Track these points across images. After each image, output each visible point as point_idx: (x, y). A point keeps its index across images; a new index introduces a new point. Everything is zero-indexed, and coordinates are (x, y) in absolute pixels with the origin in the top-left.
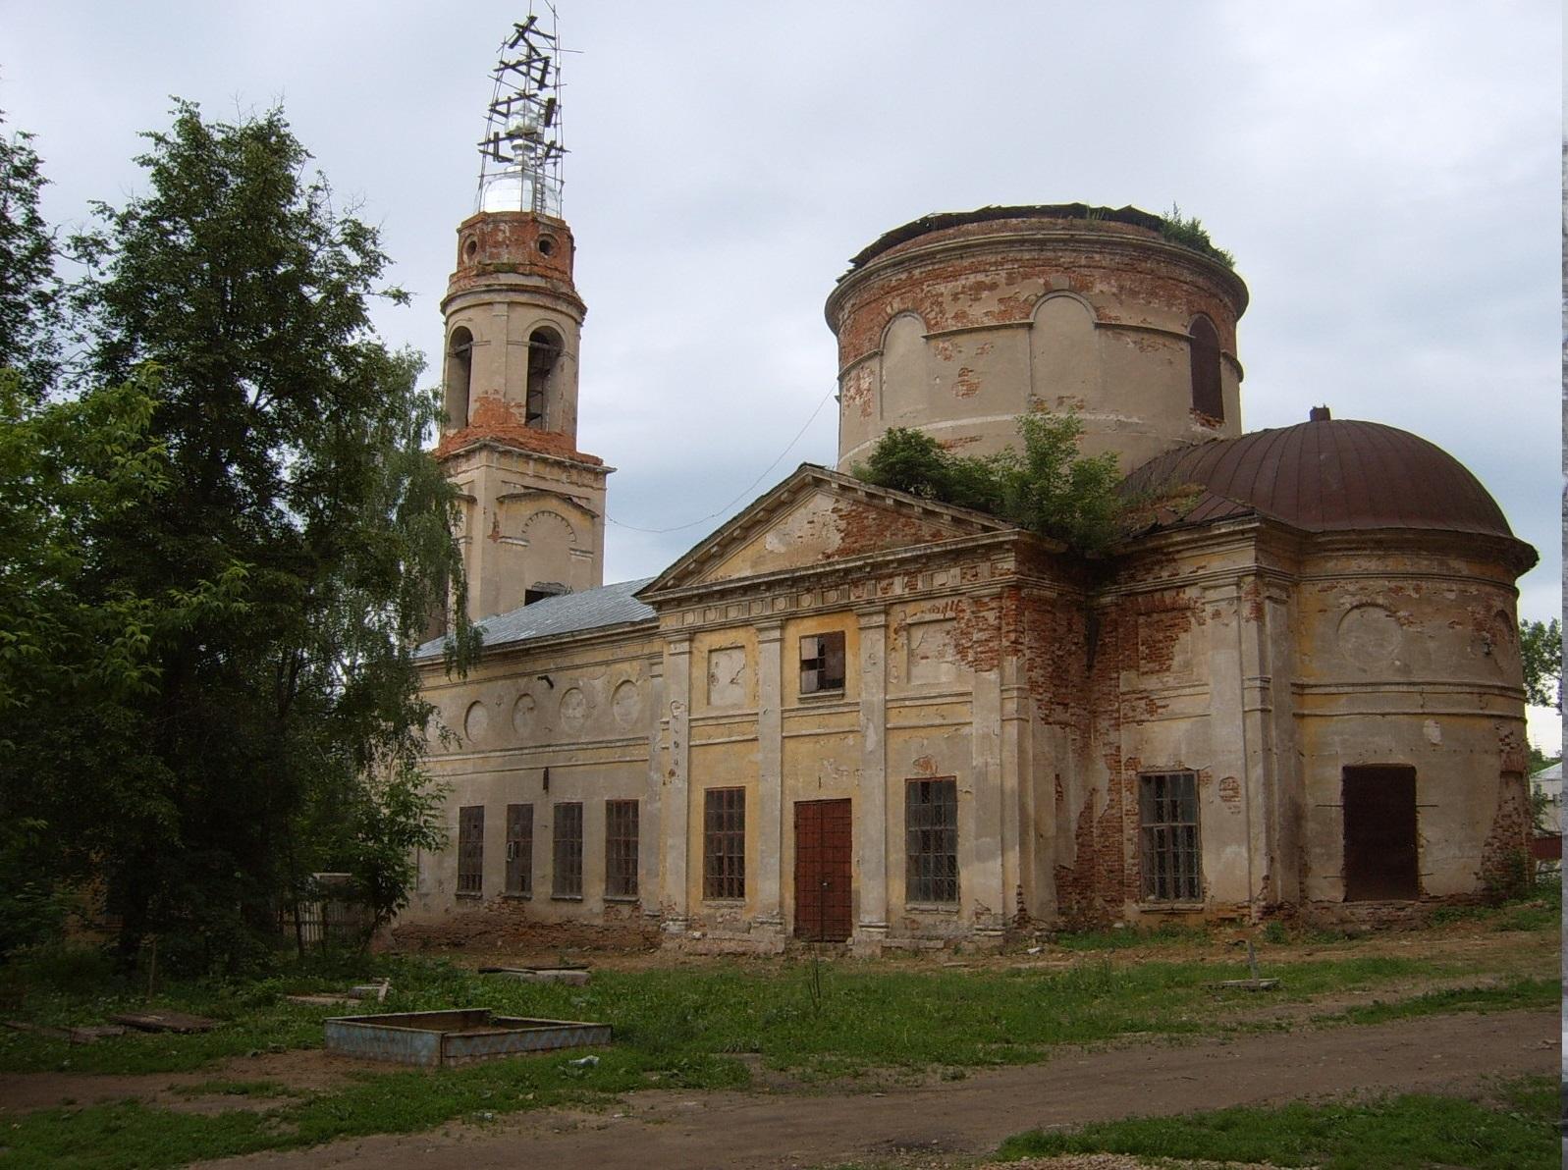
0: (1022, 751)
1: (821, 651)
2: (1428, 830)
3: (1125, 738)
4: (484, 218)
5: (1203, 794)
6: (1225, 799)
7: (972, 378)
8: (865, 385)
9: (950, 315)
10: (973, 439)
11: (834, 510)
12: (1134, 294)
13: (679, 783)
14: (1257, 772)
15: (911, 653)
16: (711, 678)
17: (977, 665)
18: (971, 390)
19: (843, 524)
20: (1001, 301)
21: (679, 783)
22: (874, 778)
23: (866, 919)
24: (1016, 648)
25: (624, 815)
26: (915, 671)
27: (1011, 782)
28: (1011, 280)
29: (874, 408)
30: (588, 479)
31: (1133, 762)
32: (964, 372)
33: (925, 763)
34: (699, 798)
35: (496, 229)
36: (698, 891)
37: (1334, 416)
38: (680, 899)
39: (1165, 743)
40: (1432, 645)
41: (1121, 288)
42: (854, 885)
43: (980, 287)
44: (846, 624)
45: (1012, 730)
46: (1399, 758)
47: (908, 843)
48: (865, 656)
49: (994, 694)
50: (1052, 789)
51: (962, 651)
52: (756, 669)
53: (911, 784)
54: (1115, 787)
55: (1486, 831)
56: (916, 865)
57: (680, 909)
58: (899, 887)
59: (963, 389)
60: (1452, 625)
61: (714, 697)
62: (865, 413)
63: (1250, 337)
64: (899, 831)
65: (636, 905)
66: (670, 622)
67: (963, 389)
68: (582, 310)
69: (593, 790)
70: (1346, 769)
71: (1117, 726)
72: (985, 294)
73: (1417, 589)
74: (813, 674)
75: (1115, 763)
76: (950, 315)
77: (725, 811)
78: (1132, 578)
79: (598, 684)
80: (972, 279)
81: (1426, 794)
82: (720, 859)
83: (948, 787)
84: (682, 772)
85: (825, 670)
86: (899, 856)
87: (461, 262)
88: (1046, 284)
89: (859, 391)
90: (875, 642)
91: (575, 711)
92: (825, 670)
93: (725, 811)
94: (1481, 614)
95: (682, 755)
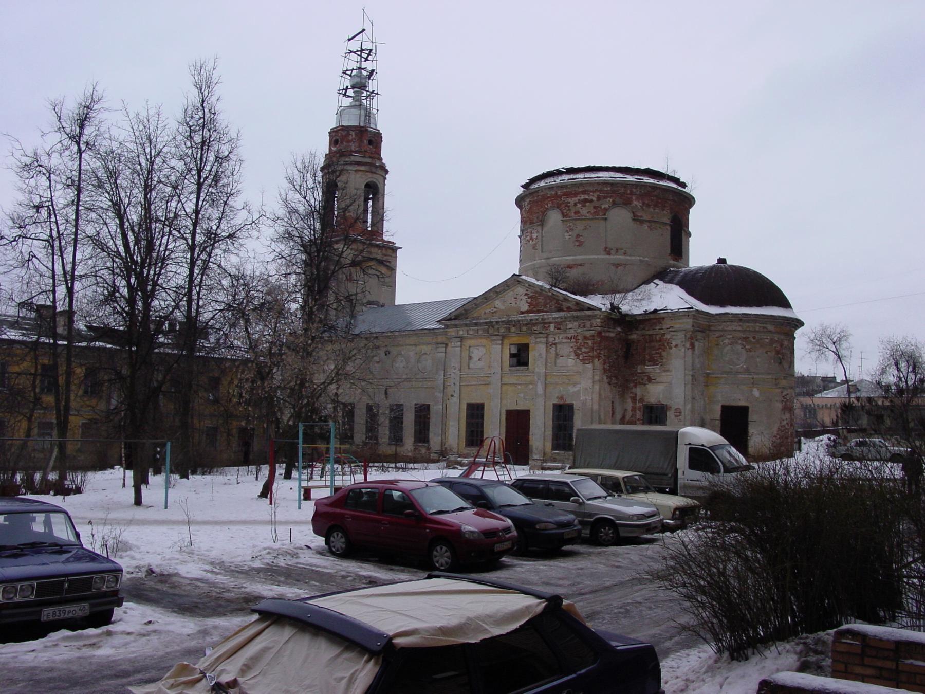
0: (600, 395)
1: (519, 350)
2: (752, 430)
3: (639, 391)
4: (344, 128)
5: (668, 414)
6: (676, 416)
7: (582, 239)
8: (535, 236)
9: (573, 211)
10: (581, 265)
11: (526, 294)
12: (648, 206)
13: (455, 400)
14: (689, 406)
15: (557, 355)
16: (470, 358)
17: (584, 361)
18: (581, 244)
19: (529, 300)
20: (595, 207)
21: (455, 400)
22: (540, 402)
23: (536, 457)
24: (599, 357)
25: (423, 413)
26: (558, 361)
27: (596, 407)
28: (599, 198)
29: (539, 247)
30: (389, 252)
31: (641, 400)
32: (578, 236)
33: (562, 398)
34: (464, 407)
35: (348, 134)
36: (463, 443)
37: (729, 262)
38: (455, 446)
39: (655, 393)
40: (758, 360)
41: (644, 203)
42: (530, 443)
43: (586, 201)
44: (531, 341)
45: (597, 387)
46: (743, 403)
47: (553, 428)
48: (537, 352)
49: (590, 374)
50: (610, 410)
51: (577, 355)
52: (490, 356)
53: (555, 405)
54: (634, 409)
55: (775, 429)
56: (556, 437)
57: (455, 450)
58: (549, 445)
59: (577, 243)
60: (766, 352)
61: (471, 365)
62: (534, 247)
63: (695, 218)
64: (550, 423)
65: (429, 449)
66: (452, 332)
67: (577, 243)
68: (387, 172)
69: (409, 400)
70: (723, 407)
71: (635, 386)
72: (588, 204)
73: (754, 338)
74: (515, 360)
75: (634, 399)
76: (573, 211)
77: (476, 412)
78: (644, 329)
79: (411, 354)
80: (583, 197)
81: (752, 417)
82: (472, 431)
83: (571, 407)
84: (456, 395)
85: (520, 358)
86: (550, 433)
87: (330, 149)
88: (613, 201)
89: (532, 239)
90: (542, 348)
91: (400, 364)
92: (520, 358)
93: (476, 412)
94: (778, 348)
95: (457, 388)
